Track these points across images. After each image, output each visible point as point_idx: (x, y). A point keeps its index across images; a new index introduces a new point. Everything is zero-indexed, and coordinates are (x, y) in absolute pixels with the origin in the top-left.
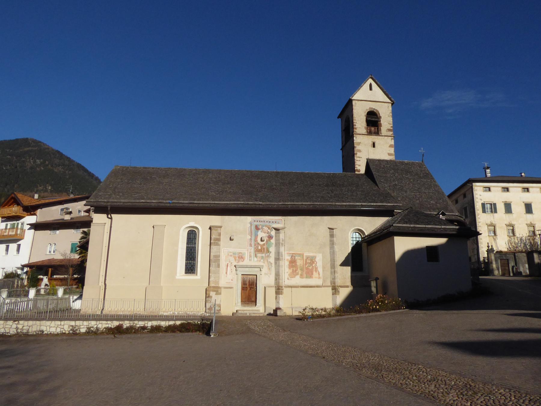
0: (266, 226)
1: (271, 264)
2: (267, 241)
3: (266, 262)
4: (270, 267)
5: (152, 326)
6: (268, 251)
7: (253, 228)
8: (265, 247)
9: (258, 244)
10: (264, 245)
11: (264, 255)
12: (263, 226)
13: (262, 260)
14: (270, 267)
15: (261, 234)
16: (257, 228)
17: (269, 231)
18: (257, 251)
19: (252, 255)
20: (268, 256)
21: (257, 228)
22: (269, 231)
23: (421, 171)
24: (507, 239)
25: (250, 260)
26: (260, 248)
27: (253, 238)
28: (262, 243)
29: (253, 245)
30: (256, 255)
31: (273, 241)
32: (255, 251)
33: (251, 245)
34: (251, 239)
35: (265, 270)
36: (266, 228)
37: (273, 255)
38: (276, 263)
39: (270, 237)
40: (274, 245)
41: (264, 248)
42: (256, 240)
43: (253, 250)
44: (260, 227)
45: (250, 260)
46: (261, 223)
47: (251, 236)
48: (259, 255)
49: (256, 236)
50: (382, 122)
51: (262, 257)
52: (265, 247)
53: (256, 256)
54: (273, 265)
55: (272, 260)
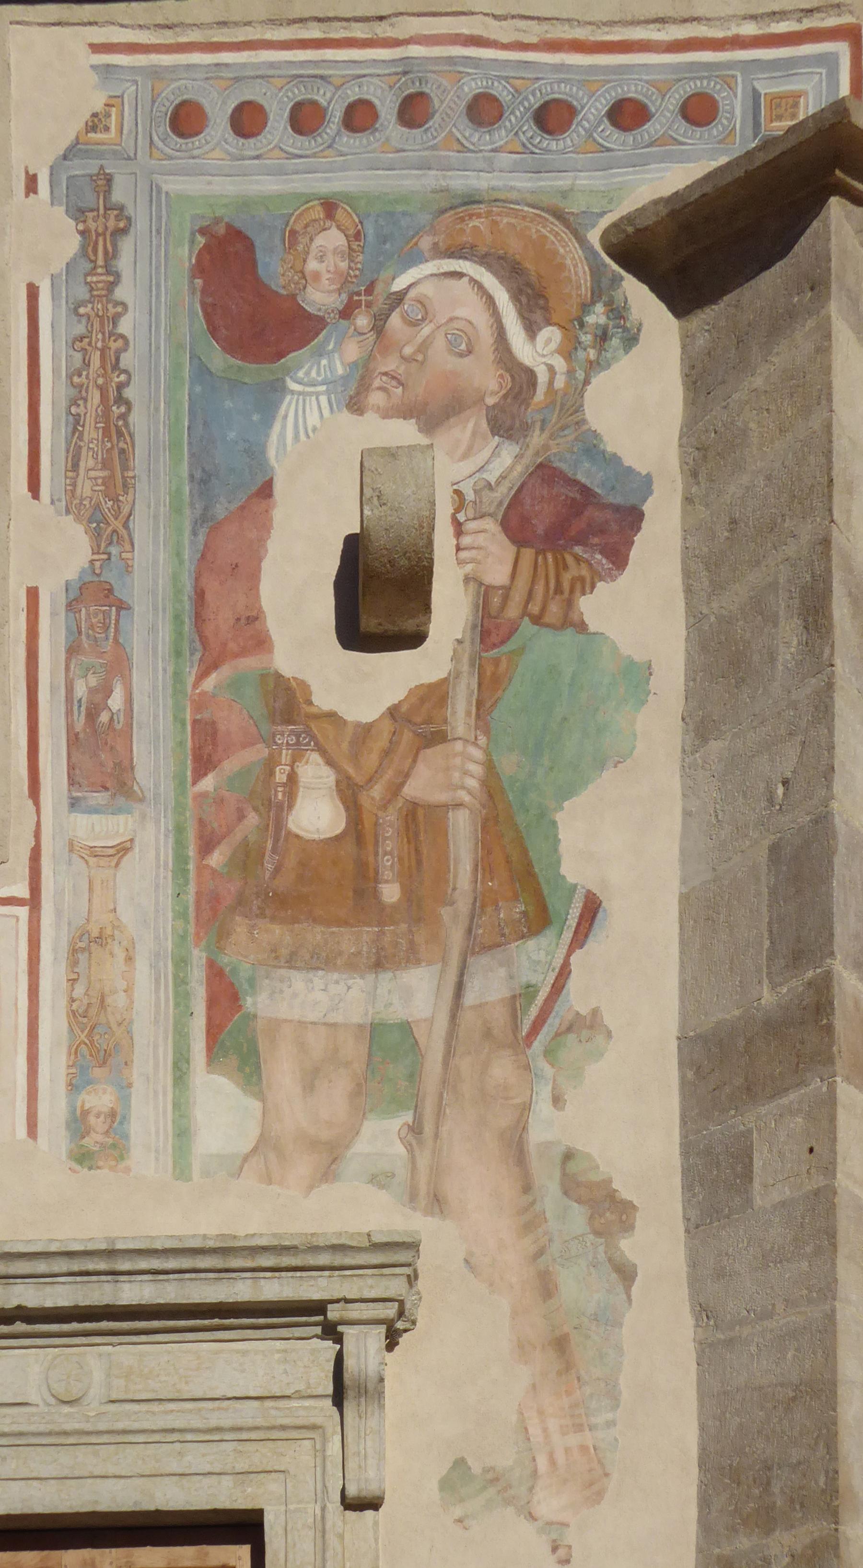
0: (461, 228)
1: (610, 1210)
2: (490, 628)
3: (477, 1180)
4: (580, 1287)
5: (188, 870)
6: (526, 893)
7: (155, 297)
8: (449, 777)
9: (286, 702)
10: (420, 721)
11: (415, 994)
12: (381, 236)
13: (381, 1138)
14: (580, 1287)
15: (322, 460)
16: (249, 310)
17: (539, 351)
18: (264, 892)
19: (148, 998)
20: (537, 1023)
21: (249, 310)
22: (539, 351)
23: (798, 673)
24: (401, 1328)
25: (96, 1144)
26: (317, 814)
27: (155, 564)
28: (364, 688)
29: (155, 753)
30: (224, 997)
31: (641, 609)
32: (211, 914)
33: (100, 762)
34: (97, 598)
35: (451, 1379)
36: (454, 300)
37: (638, 986)
38: (717, 1176)
39: (571, 521)
40: (657, 727)
41: (422, 824)
42: (219, 622)
43: (145, 897)
44: (320, 271)
45: (96, 1144)
46: (350, 169)
47: (108, 529)
48: (311, 1000)
49: (232, 506)
50: (625, 213)
51: (388, 1045)
52: (449, 777)
53: (229, 1029)
54: (659, 1242)
55: (624, 1109)
